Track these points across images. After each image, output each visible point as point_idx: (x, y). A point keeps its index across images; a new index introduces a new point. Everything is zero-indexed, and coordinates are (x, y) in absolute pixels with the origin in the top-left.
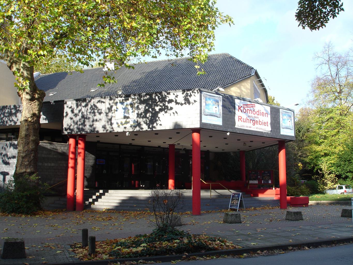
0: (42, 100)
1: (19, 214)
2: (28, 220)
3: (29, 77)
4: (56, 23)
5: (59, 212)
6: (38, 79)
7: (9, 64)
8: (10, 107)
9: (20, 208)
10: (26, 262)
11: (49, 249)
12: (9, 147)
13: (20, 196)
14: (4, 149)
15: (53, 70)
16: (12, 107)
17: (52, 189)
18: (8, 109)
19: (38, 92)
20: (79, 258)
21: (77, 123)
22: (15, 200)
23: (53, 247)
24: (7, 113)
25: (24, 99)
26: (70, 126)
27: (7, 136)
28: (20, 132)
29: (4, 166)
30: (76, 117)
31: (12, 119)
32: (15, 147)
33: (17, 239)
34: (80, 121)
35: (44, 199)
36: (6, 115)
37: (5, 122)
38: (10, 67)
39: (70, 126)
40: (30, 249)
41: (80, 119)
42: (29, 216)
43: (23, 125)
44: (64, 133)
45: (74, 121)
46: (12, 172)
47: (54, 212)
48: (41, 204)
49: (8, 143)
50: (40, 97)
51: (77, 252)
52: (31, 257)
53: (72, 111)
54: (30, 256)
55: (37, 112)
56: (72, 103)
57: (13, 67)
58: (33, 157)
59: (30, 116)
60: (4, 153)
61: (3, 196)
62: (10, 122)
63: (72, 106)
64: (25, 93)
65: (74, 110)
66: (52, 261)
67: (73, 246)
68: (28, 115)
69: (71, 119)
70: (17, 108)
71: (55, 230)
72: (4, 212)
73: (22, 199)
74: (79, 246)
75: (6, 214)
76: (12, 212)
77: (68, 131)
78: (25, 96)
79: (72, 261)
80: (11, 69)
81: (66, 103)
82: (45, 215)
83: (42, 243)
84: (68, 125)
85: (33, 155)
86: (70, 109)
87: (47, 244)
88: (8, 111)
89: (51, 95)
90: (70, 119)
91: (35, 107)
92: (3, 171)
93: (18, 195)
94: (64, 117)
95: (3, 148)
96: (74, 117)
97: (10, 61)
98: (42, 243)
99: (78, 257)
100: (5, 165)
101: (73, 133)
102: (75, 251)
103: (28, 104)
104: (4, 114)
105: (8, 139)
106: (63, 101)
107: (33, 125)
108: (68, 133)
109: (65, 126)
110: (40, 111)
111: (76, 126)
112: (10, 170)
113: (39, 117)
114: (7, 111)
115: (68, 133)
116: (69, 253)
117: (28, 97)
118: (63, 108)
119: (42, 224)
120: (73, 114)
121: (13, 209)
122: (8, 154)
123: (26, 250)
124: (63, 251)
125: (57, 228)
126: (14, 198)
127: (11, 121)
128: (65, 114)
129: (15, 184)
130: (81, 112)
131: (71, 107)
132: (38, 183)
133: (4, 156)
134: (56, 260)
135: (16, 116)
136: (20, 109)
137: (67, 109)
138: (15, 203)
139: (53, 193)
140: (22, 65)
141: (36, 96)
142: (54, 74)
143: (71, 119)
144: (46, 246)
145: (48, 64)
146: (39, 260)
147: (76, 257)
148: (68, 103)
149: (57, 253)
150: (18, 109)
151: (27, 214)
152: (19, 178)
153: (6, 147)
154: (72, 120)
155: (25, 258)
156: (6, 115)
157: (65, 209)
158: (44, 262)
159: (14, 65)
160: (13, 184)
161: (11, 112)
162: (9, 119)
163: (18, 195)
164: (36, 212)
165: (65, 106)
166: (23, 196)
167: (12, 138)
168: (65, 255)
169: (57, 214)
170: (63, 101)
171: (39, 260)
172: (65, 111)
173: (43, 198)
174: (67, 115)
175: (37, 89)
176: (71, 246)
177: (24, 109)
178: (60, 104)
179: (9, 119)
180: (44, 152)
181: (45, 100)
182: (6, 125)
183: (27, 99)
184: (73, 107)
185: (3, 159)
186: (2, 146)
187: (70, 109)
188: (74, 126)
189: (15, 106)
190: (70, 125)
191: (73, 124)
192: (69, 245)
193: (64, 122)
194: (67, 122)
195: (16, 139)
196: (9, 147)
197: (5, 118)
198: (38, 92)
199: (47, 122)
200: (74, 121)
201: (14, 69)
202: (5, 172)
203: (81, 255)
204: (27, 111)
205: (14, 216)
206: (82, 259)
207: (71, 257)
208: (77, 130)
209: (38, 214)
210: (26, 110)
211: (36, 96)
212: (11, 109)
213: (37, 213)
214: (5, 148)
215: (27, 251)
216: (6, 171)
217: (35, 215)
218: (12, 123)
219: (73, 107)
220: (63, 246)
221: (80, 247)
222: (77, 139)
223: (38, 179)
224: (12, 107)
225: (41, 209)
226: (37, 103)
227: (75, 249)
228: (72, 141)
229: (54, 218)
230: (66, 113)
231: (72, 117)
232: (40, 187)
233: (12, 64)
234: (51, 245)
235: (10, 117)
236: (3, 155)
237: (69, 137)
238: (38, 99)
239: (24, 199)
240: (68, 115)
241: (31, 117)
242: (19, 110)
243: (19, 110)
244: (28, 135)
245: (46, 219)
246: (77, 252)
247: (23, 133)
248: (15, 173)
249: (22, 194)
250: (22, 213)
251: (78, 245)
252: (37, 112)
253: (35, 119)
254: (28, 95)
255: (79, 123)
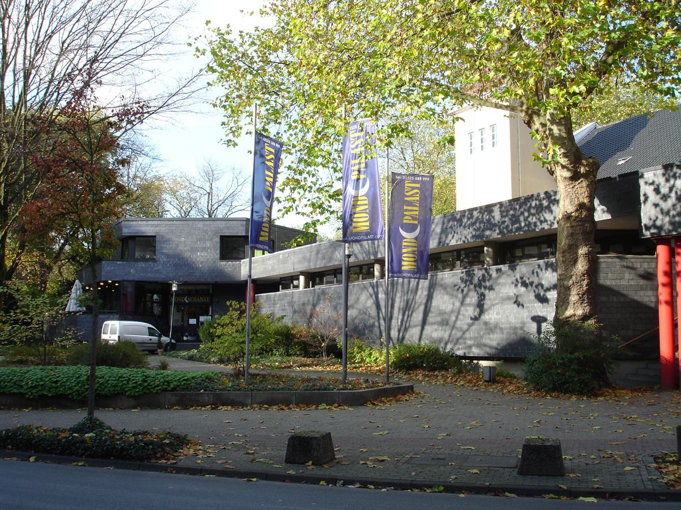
0: (595, 176)
1: (565, 393)
2: (582, 406)
3: (564, 135)
4: (595, 27)
5: (646, 391)
6: (593, 136)
7: (527, 118)
8: (539, 195)
9: (566, 382)
10: (563, 484)
11: (610, 461)
12: (544, 269)
13: (566, 360)
14: (535, 275)
15: (621, 115)
16: (542, 196)
17: (631, 347)
18: (536, 200)
19: (584, 162)
20: (666, 483)
21: (668, 213)
22: (557, 368)
23: (619, 459)
24: (534, 208)
25: (559, 178)
26: (654, 221)
27: (540, 249)
28: (558, 241)
29: (538, 305)
30: (665, 200)
31: (544, 218)
32: (553, 267)
33: (548, 440)
34: (674, 209)
35: (613, 366)
36: (533, 211)
37: (532, 226)
38: (529, 124)
39: (654, 221)
40: (574, 461)
41: (674, 205)
42: (585, 398)
43: (563, 228)
44: (644, 236)
45: (662, 210)
46: (551, 317)
47: (636, 390)
48: (608, 375)
49: (541, 262)
50: (589, 171)
51: (664, 471)
52: (574, 475)
53: (657, 191)
54: (571, 473)
55: (586, 201)
56: (654, 174)
57: (533, 121)
58: (587, 285)
59: (575, 208)
60: (536, 281)
61: (535, 361)
62: (541, 224)
63: (656, 179)
64: (560, 168)
65: (660, 187)
66: (612, 486)
67: (660, 458)
68: (570, 207)
69: (656, 205)
70: (551, 196)
71: (630, 427)
72: (539, 390)
73: (570, 366)
74: (671, 459)
75: (542, 394)
76: (554, 389)
77: (653, 231)
78: (562, 174)
79: (651, 487)
80: (530, 127)
81: (642, 176)
82: (616, 396)
83: (599, 450)
84: (650, 219)
85: (586, 282)
86: (652, 187)
87: (610, 452)
88: (536, 204)
89: (620, 163)
90: (653, 207)
91: (581, 190)
92: (536, 314)
93: (563, 359)
94: (640, 204)
95: (533, 273)
96: (661, 203)
97: (527, 113)
98: (599, 450)
99: (665, 481)
100: (540, 304)
101: (663, 234)
102: (660, 468)
103: (568, 187)
104: (529, 211)
105: (540, 257)
106: (637, 172)
107: (581, 225)
108: (652, 234)
109: (645, 220)
110: (591, 198)
111: (667, 219)
112: (547, 312)
113: (592, 209)
114: (533, 204)
115: (652, 234)
116: (649, 473)
117: (568, 174)
118: (638, 187)
119: (607, 414)
120: (658, 197)
121: (554, 384)
122: (543, 282)
123: (565, 462)
124: (638, 467)
125: (633, 423)
126: (554, 364)
127: (541, 222)
128: (642, 198)
129: (557, 339)
130: (674, 189)
131: (653, 183)
132: (599, 336)
133: (537, 286)
134: (620, 484)
135: (551, 212)
136: (557, 198)
137: (645, 189)
138: (558, 373)
139: (630, 353)
140: (548, 117)
141: (582, 170)
142: (625, 121)
143: (656, 205)
144: (606, 456)
145: (590, 107)
146: (587, 483)
147: (660, 480)
148: (646, 175)
149: (625, 471)
150: (553, 198)
151: (580, 393)
152: (562, 327)
153: (539, 271)
154: (658, 209)
155: (562, 475)
156: (533, 211)
157: (659, 386)
158: (596, 486)
159: (535, 118)
160: (553, 339)
161: (541, 205)
162: (539, 219)
163: (563, 359)
164: (600, 390)
165: (641, 182)
166: (571, 361)
167: (548, 253)
168: (641, 475)
169: (640, 394)
170: (637, 172)
171: (587, 483)
172: (642, 193)
173: (610, 363)
174: (646, 199)
175: (582, 159)
176: (656, 459)
177: (562, 197)
178: (631, 180)
179: (539, 219)
180: (610, 275)
181: (602, 174)
182: (535, 230)
183: (565, 178)
184: (657, 183)
185: (537, 291)
186: (531, 269)
187: (652, 187)
188: (662, 220)
189: (546, 193)
190: (653, 218)
191: (660, 217)
192: (652, 456)
193: (642, 214)
194: (647, 213)
195: (554, 254)
196: (544, 269)
197: (531, 217)
198: (584, 162)
199: (608, 217)
200: (662, 210)
201: (537, 125)
202: (539, 317)
203: (672, 477)
204: (568, 201)
205: (558, 397)
206: (672, 485)
207: (650, 480)
208: (670, 228)
209: (602, 395)
210: (568, 197)
211: (582, 170)
212: (540, 201)
213: (601, 392)
214: (537, 272)
215: (567, 464)
216: (541, 314)
217: (596, 395)
218: (546, 226)
219: (657, 183)
220: (640, 458)
221: (673, 463)
222: (673, 245)
223: (600, 328)
224: (542, 196)
225: (609, 385)
226: (584, 184)
227: (663, 465)
228: (661, 250)
229: (632, 403)
230: (645, 195)
231: (657, 202)
232: (604, 344)
233: (531, 117)
234: (617, 455)
235: (541, 215)
236: (534, 285)
237: (655, 241)
238: (585, 176)
239: (574, 366)
240: (649, 200)
241: (577, 210)
242: (555, 199)
243: (555, 199)
244: (572, 245)
245: (617, 405)
246: (664, 471)
247: (563, 241)
248: (556, 319)
249: (569, 356)
250: (571, 392)
251: (671, 457)
252: (586, 201)
253: (584, 213)
254: (565, 170)
255: (672, 213)
